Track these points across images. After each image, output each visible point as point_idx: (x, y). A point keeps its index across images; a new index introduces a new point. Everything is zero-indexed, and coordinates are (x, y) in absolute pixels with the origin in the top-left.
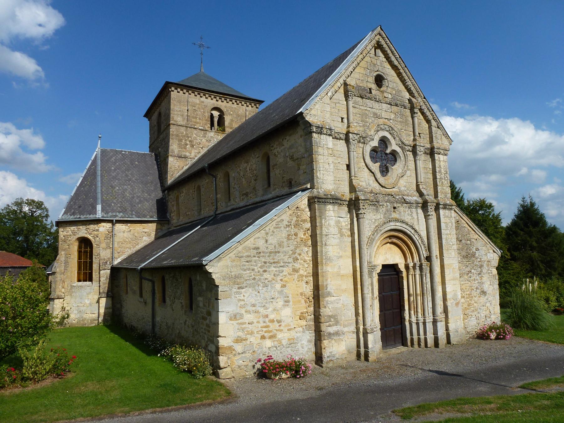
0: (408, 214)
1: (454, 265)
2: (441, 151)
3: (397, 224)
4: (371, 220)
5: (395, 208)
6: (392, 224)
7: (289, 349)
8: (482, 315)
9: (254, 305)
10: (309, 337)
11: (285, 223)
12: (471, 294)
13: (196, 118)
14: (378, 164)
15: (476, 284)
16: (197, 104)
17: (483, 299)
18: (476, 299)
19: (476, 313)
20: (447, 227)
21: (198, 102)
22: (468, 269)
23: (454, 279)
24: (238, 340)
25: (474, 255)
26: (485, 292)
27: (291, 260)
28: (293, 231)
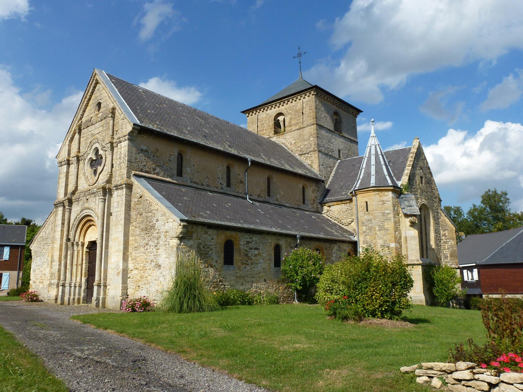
5: (87, 199)
6: (84, 211)
8: (154, 289)
10: (370, 318)
11: (52, 222)
12: (145, 267)
13: (263, 130)
17: (157, 272)
18: (150, 272)
19: (148, 286)
20: (118, 205)
21: (264, 116)
22: (146, 241)
25: (153, 227)
26: (160, 265)
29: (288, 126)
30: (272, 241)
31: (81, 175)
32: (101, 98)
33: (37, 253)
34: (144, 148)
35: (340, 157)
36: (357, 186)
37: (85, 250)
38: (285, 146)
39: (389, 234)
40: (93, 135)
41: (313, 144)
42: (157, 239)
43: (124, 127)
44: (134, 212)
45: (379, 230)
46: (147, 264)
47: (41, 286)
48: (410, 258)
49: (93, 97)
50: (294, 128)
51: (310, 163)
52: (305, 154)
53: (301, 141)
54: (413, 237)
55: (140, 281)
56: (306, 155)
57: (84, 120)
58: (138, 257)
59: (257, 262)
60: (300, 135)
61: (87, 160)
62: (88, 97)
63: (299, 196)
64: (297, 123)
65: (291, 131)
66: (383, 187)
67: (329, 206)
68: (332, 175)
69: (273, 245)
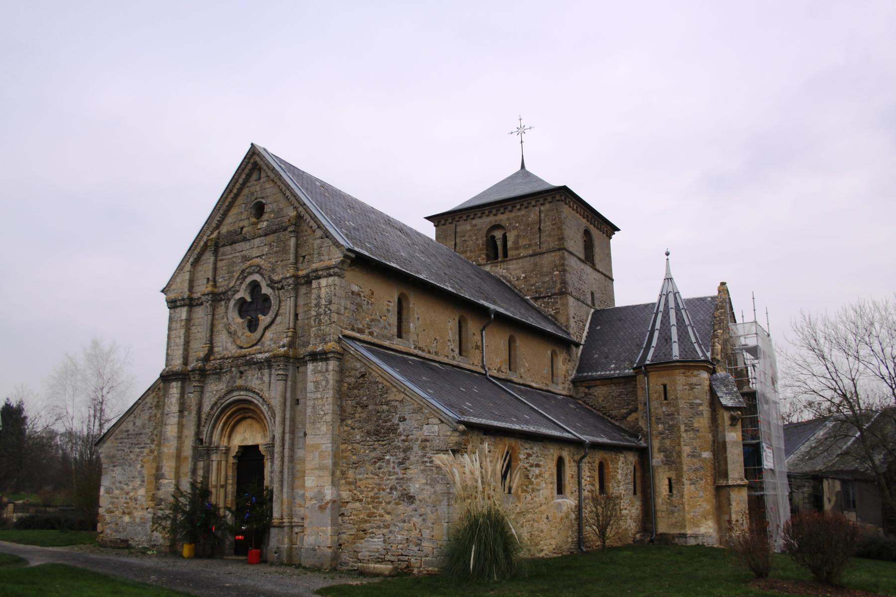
0: (257, 378)
1: (324, 447)
2: (320, 273)
3: (242, 393)
4: (212, 392)
5: (241, 373)
6: (235, 394)
7: (140, 528)
9: (120, 482)
11: (149, 405)
12: (378, 498)
14: (261, 317)
15: (392, 481)
16: (467, 231)
17: (404, 509)
20: (317, 387)
21: (468, 227)
22: (377, 454)
23: (321, 468)
24: (110, 511)
25: (393, 429)
26: (411, 497)
27: (149, 441)
28: (154, 411)
29: (512, 249)
30: (553, 452)
31: (220, 326)
32: (263, 195)
33: (114, 460)
34: (356, 288)
35: (594, 304)
36: (649, 357)
37: (231, 460)
38: (508, 281)
39: (699, 438)
40: (245, 259)
41: (559, 282)
42: (405, 451)
43: (325, 253)
44: (350, 402)
45: (686, 431)
46: (383, 493)
47: (127, 519)
48: (730, 476)
49: (246, 191)
50: (523, 253)
51: (553, 313)
52: (544, 297)
53: (536, 275)
54: (735, 443)
55: (366, 521)
56: (546, 300)
57: (224, 229)
58: (360, 480)
59: (538, 488)
60: (536, 265)
61: (232, 303)
62: (235, 191)
63: (546, 370)
64: (530, 245)
65: (518, 258)
66: (691, 361)
67: (589, 387)
68: (585, 334)
69: (556, 458)
